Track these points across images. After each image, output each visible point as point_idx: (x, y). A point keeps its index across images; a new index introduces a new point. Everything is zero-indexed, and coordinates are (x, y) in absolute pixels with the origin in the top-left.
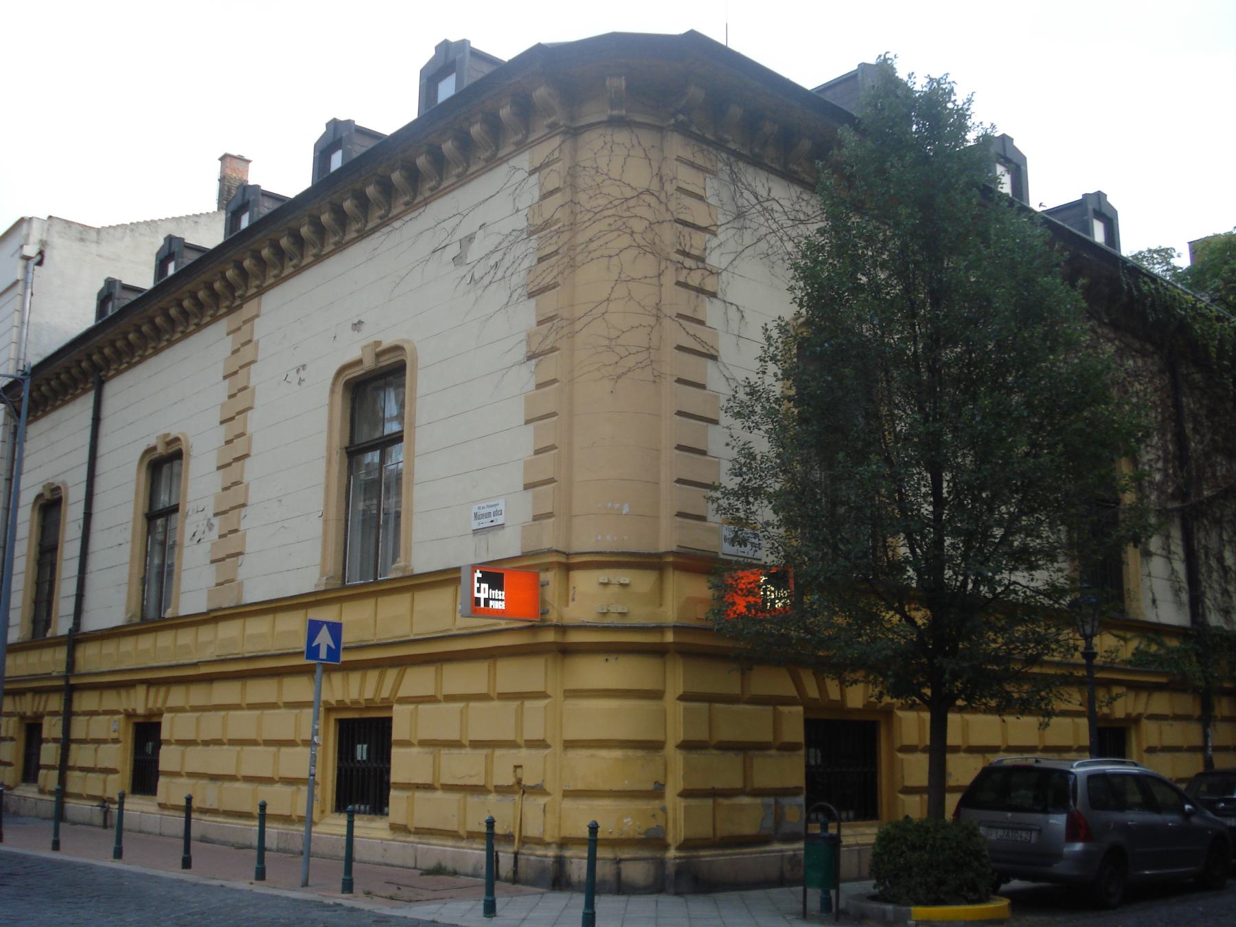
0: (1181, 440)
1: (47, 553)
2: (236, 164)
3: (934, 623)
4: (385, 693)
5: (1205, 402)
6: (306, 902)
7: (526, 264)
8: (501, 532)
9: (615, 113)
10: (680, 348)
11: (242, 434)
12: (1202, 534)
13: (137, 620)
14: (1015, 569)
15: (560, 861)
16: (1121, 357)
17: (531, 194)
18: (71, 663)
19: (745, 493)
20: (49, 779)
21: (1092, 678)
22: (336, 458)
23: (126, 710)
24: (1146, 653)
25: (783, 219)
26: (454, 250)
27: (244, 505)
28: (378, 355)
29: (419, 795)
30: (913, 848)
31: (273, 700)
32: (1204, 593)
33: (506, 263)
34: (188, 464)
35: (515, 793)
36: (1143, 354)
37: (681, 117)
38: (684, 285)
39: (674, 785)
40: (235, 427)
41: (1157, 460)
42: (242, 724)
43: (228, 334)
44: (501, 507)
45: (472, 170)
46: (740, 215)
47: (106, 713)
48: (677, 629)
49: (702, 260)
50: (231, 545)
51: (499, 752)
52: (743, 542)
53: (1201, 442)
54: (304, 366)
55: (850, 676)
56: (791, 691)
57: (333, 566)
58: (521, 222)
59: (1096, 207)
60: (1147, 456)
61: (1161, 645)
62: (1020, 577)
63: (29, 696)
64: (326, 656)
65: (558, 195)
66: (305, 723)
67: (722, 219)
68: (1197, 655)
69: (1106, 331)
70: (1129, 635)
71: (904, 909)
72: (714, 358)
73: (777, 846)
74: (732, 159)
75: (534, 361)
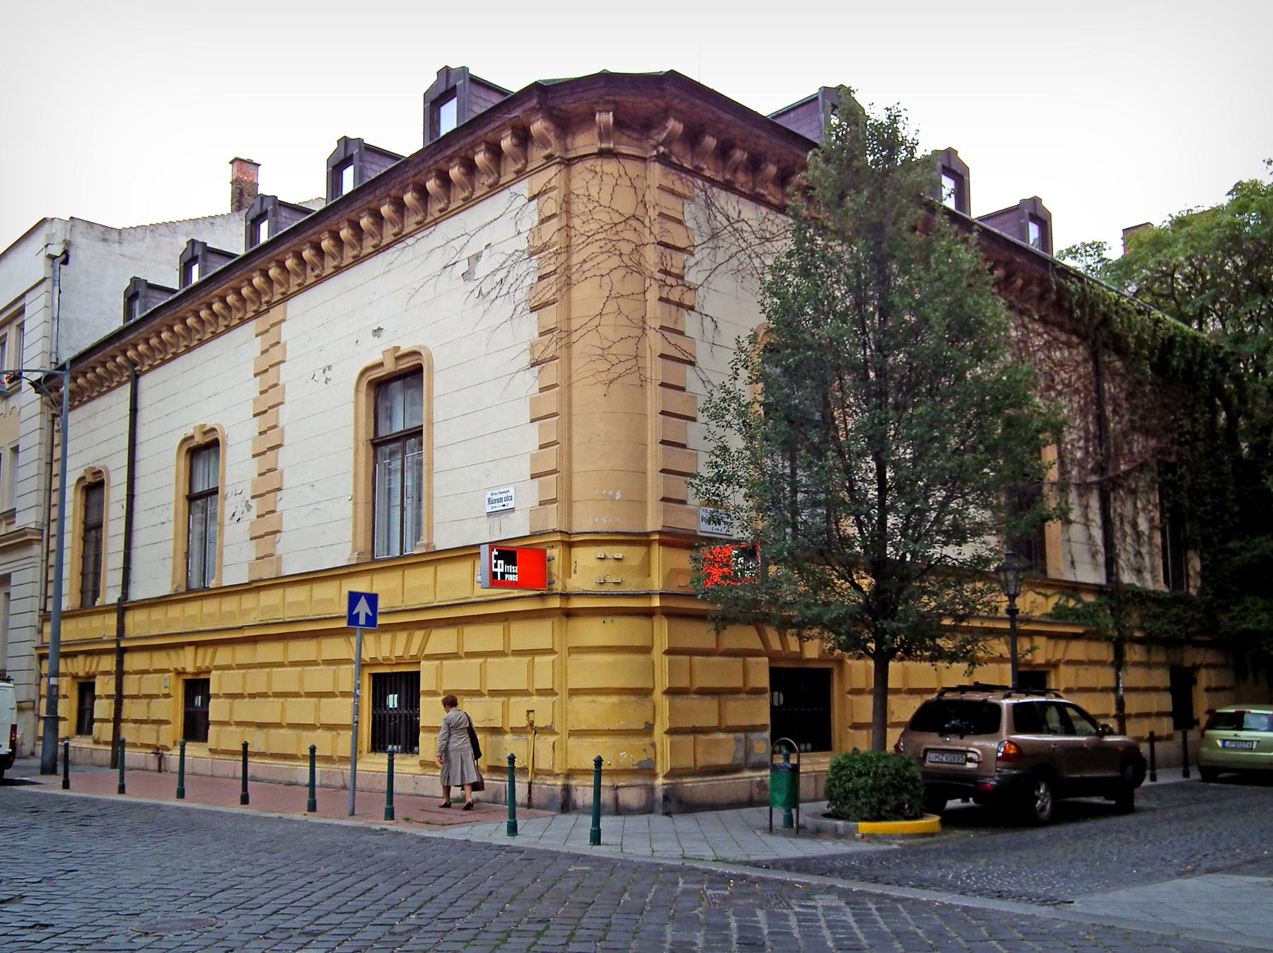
0: (1101, 421)
1: (92, 529)
2: (246, 167)
3: (877, 590)
4: (413, 651)
5: (1124, 386)
6: (355, 828)
7: (528, 281)
8: (512, 515)
9: (604, 146)
11: (275, 427)
12: (1118, 504)
14: (946, 544)
15: (567, 789)
16: (1049, 350)
17: (531, 217)
18: (56, 633)
20: (104, 731)
21: (1016, 627)
22: (362, 449)
24: (1066, 608)
25: (751, 238)
26: (463, 267)
27: (279, 489)
28: (397, 359)
30: (859, 775)
32: (1118, 555)
33: (510, 280)
34: (225, 451)
35: (528, 733)
36: (1069, 345)
37: (662, 149)
40: (269, 419)
41: (1080, 438)
42: (285, 679)
43: (257, 336)
44: (511, 493)
46: (714, 236)
48: (663, 595)
49: (682, 278)
50: (268, 524)
51: (513, 699)
52: (718, 522)
53: (1119, 423)
54: (329, 367)
55: (807, 633)
56: (758, 645)
57: (363, 543)
59: (1034, 212)
60: (1070, 436)
61: (1079, 600)
62: (951, 551)
63: (81, 658)
65: (556, 220)
66: (346, 677)
67: (698, 241)
68: (1112, 609)
69: (1036, 326)
70: (1049, 592)
71: (852, 824)
72: (692, 364)
73: (747, 774)
74: (707, 185)
75: (537, 368)
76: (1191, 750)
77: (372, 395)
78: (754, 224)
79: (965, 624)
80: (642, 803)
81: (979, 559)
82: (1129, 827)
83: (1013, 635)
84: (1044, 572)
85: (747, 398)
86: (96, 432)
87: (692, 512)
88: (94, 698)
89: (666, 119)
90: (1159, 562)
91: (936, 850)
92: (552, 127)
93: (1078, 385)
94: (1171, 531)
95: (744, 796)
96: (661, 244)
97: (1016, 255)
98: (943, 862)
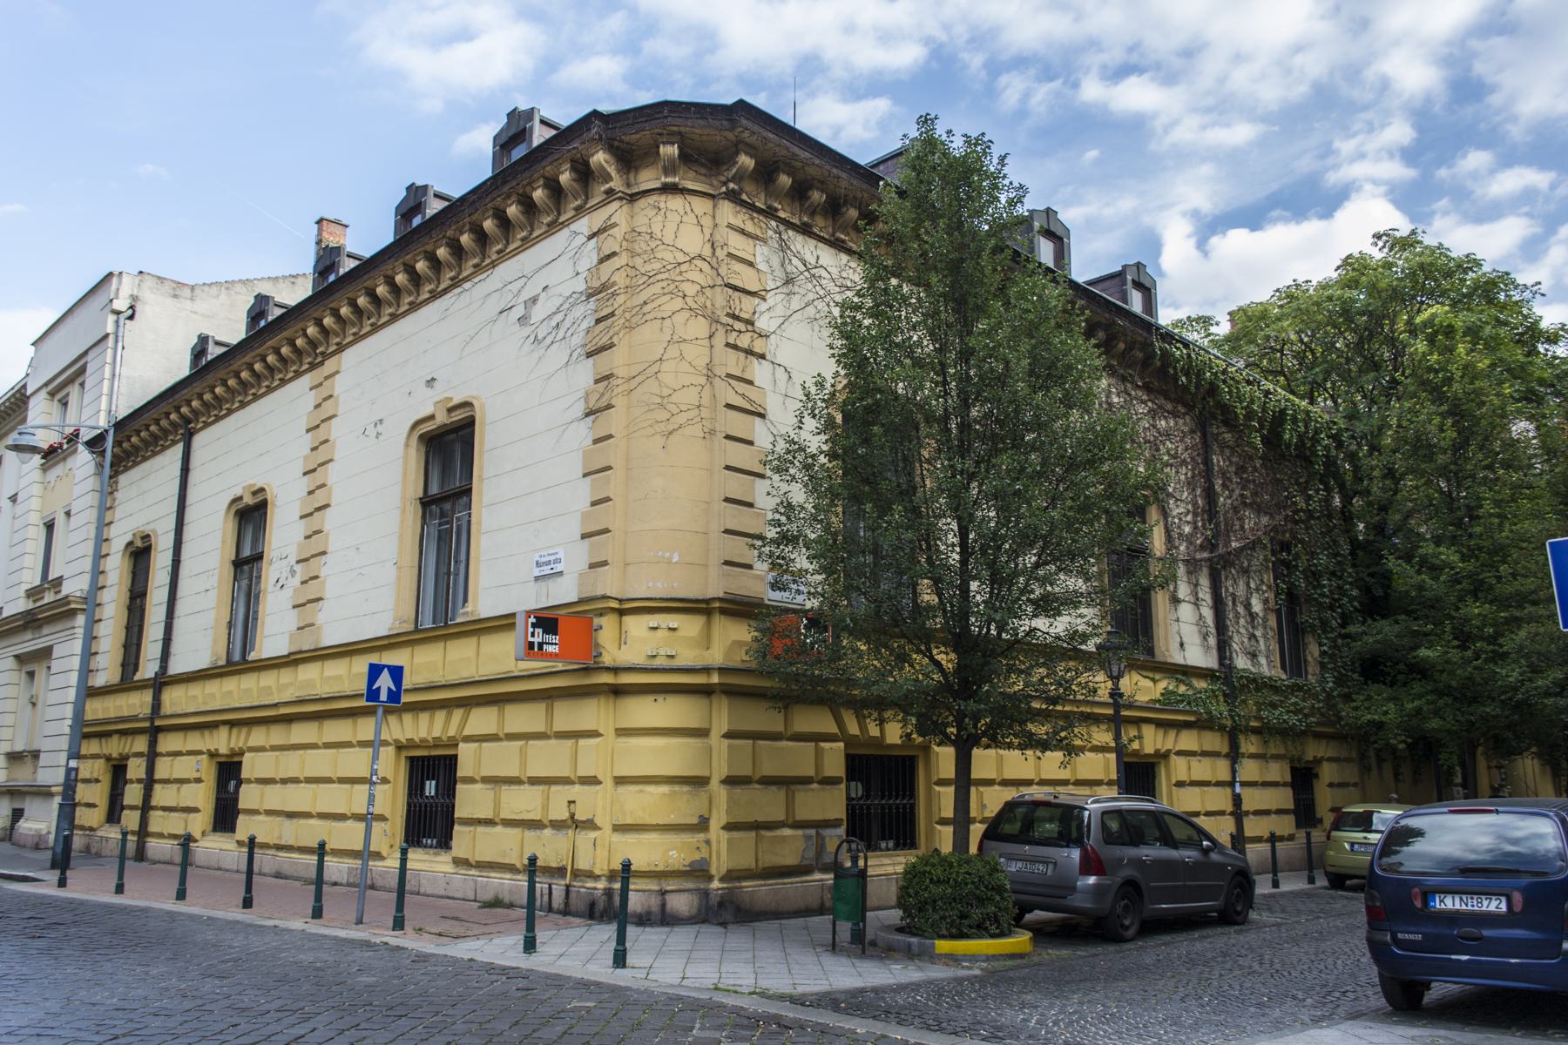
3: (960, 668)
4: (451, 733)
6: (352, 942)
7: (585, 325)
8: (560, 580)
9: (669, 180)
10: (728, 406)
11: (323, 485)
12: (1230, 582)
13: (222, 662)
14: (1035, 616)
17: (589, 258)
18: (157, 705)
19: (786, 539)
21: (1120, 715)
23: (396, 741)
25: (831, 286)
26: (519, 311)
27: (324, 553)
28: (450, 410)
29: (480, 829)
31: (542, 729)
32: (1231, 638)
33: (567, 324)
35: (568, 827)
37: (731, 185)
38: (735, 347)
39: (717, 820)
42: (318, 762)
44: (561, 555)
45: (535, 234)
47: (190, 753)
48: (722, 670)
49: (750, 322)
50: (312, 591)
51: (554, 788)
52: (784, 588)
56: (833, 728)
58: (580, 286)
61: (1190, 686)
62: (1041, 623)
63: (115, 738)
64: (386, 695)
68: (1225, 695)
72: (762, 416)
73: (817, 876)
74: (782, 228)
76: (1315, 852)
77: (423, 450)
78: (834, 271)
79: (1059, 708)
80: (694, 911)
81: (1074, 635)
82: (1251, 949)
83: (1117, 722)
84: (1150, 651)
85: (813, 450)
86: (147, 495)
87: (758, 577)
88: (240, 782)
89: (737, 153)
90: (1274, 646)
91: (1023, 979)
92: (612, 160)
93: (1186, 455)
94: (1287, 613)
95: (814, 902)
96: (728, 285)
97: (1117, 321)
98: (1028, 998)
